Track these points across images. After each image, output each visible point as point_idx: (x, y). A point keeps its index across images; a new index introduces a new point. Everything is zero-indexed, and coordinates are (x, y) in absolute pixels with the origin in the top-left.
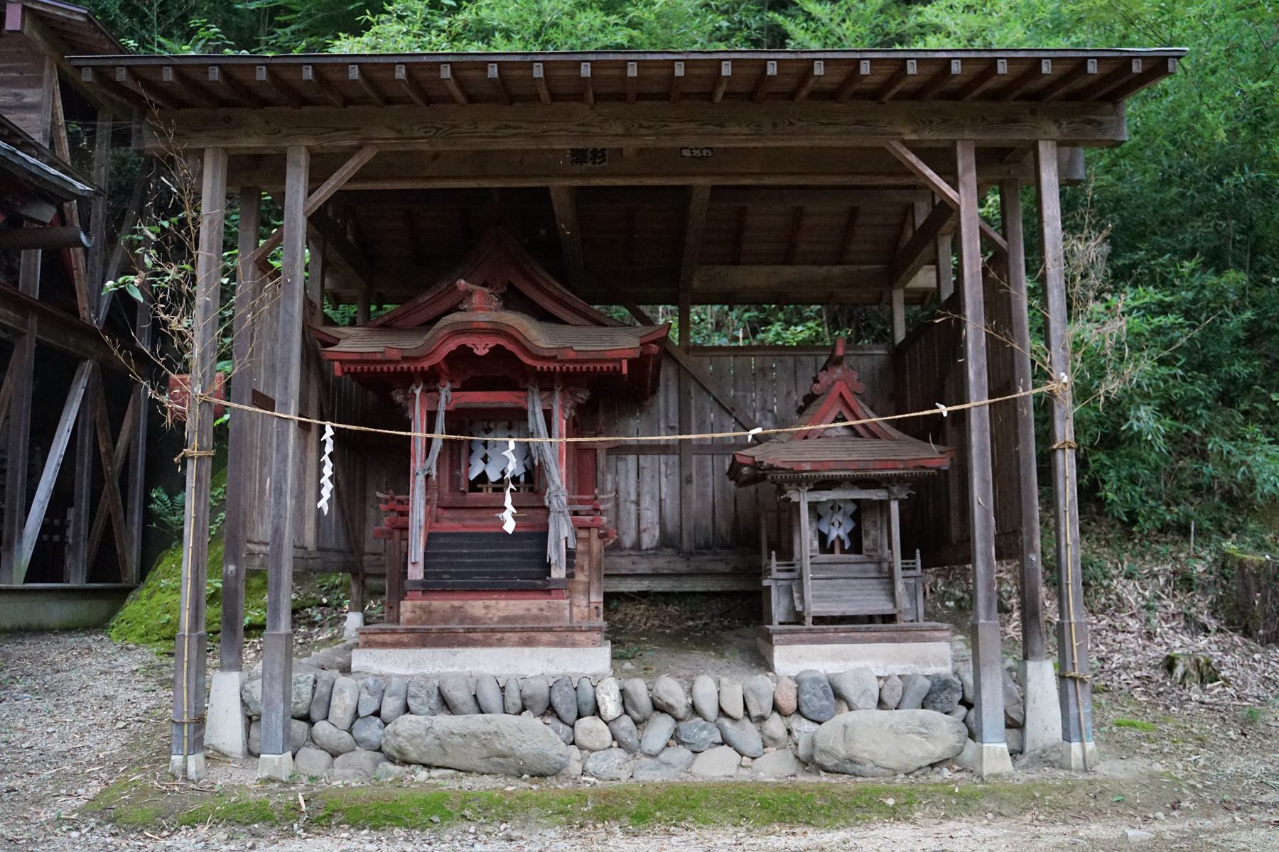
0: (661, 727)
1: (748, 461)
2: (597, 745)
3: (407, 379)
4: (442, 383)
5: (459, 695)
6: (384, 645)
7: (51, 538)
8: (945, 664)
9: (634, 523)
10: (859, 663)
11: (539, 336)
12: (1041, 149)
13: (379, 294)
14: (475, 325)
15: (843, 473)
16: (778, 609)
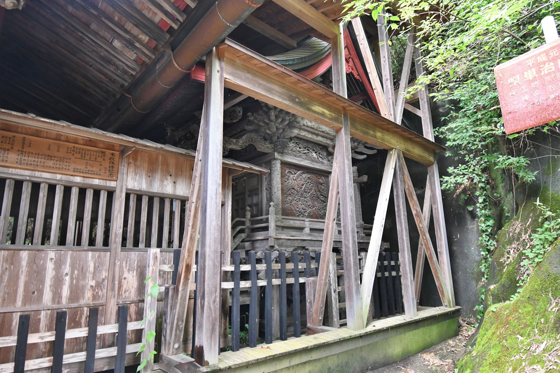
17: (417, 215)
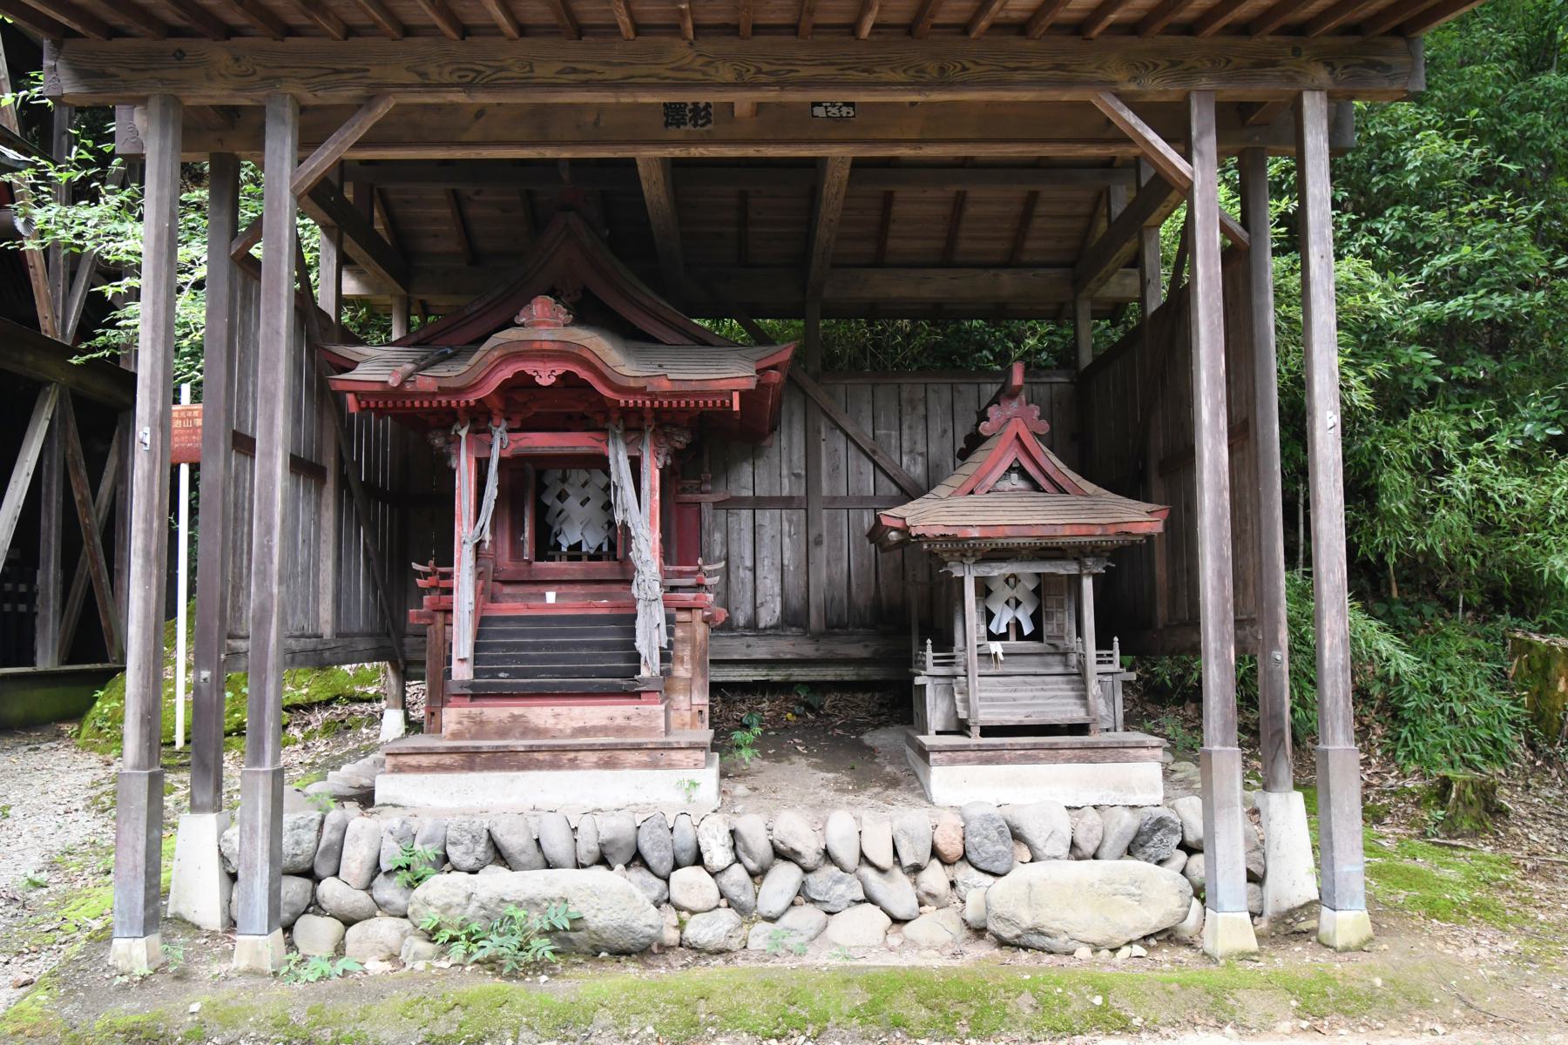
0: (784, 878)
1: (898, 524)
2: (698, 905)
3: (445, 419)
4: (496, 420)
5: (513, 841)
6: (419, 769)
7: (15, 608)
8: (1154, 790)
9: (749, 594)
10: (1041, 790)
11: (622, 364)
12: (1305, 102)
13: (422, 302)
14: (537, 346)
15: (1021, 541)
16: (936, 712)
17: (84, 502)
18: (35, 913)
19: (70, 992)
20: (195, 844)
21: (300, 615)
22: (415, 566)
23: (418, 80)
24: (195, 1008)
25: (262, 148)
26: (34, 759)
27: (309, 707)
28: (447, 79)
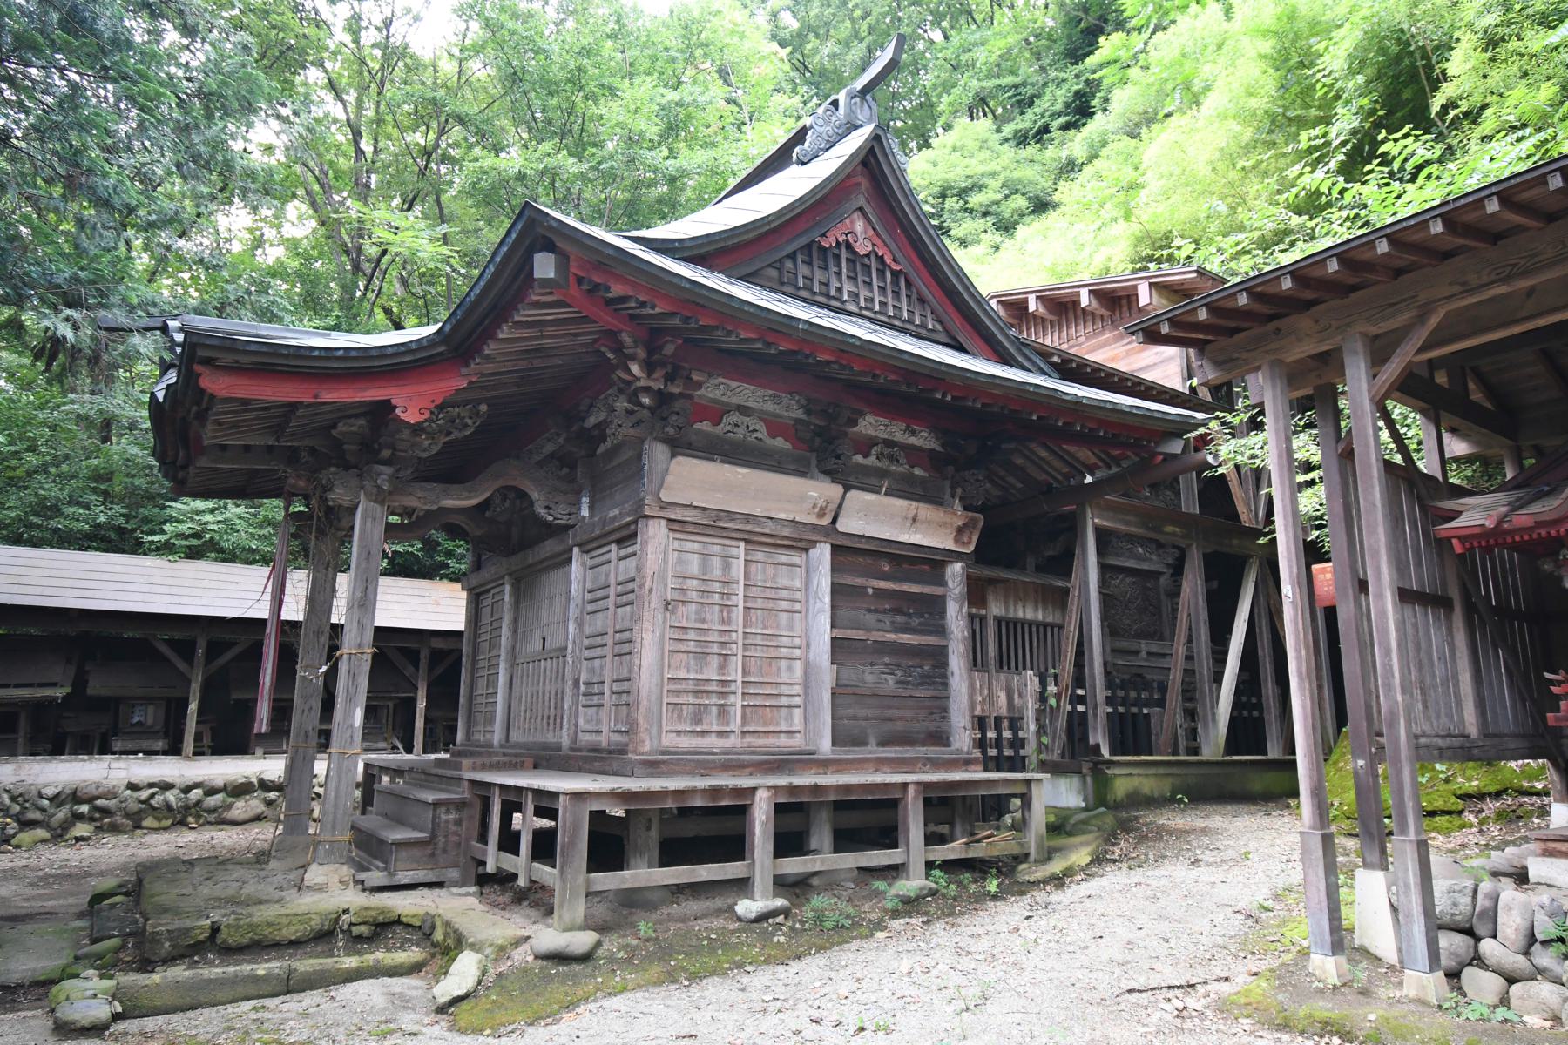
18: (1263, 928)
19: (1282, 985)
20: (1371, 898)
21: (1444, 719)
22: (1547, 675)
23: (1460, 289)
24: (1372, 1017)
25: (1344, 375)
26: (1267, 821)
27: (1481, 797)
28: (1485, 279)
